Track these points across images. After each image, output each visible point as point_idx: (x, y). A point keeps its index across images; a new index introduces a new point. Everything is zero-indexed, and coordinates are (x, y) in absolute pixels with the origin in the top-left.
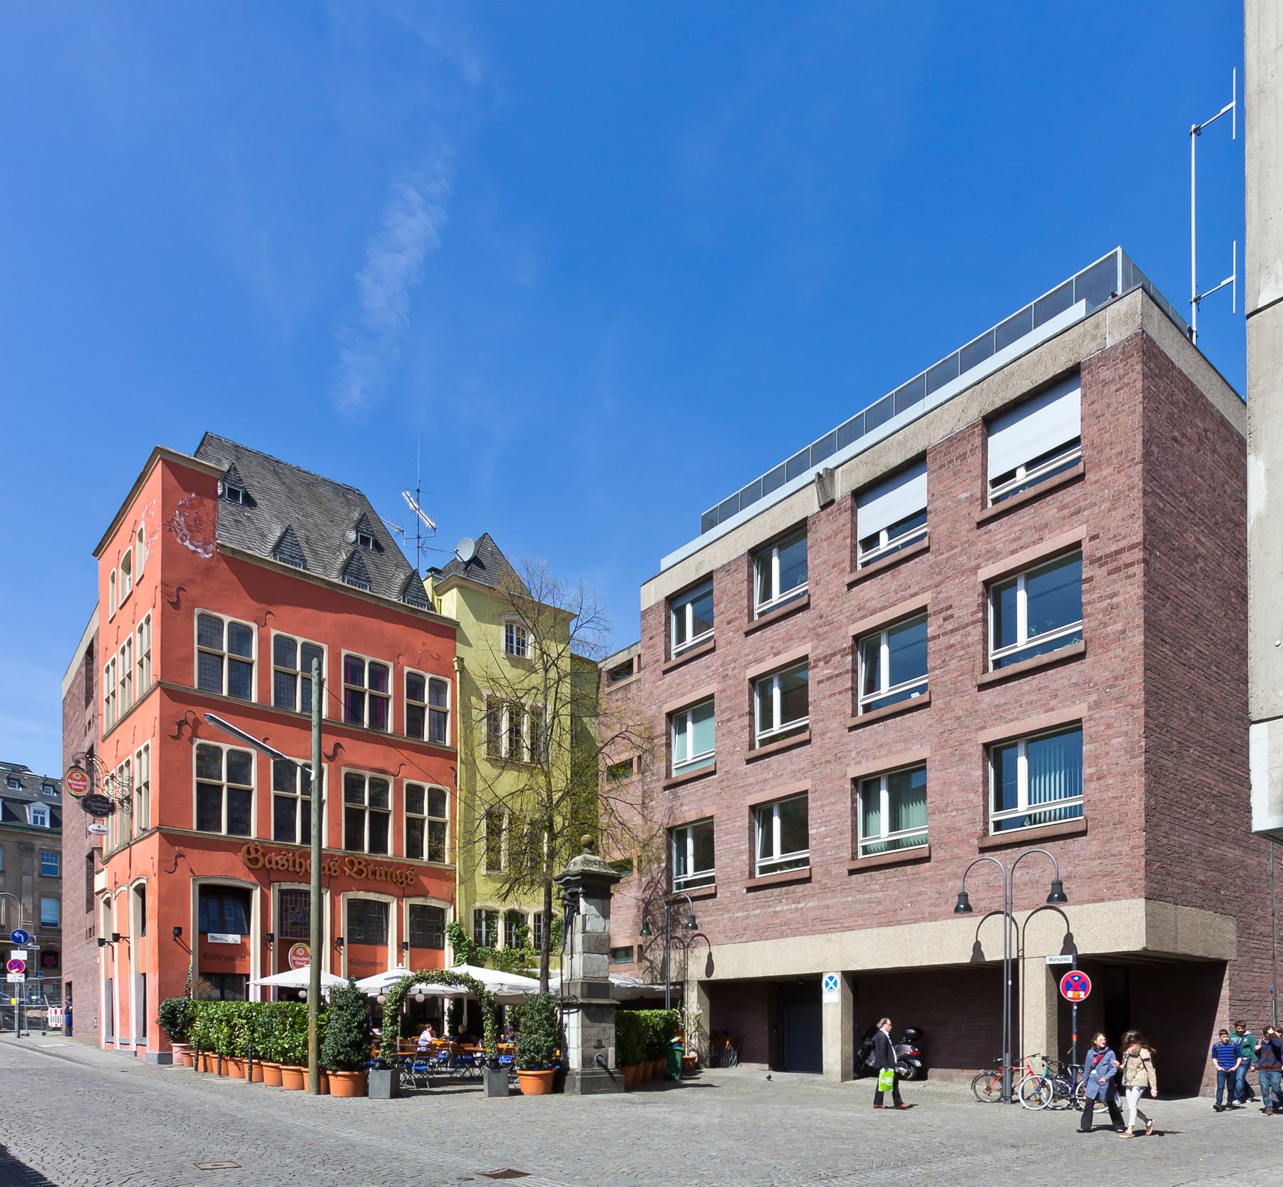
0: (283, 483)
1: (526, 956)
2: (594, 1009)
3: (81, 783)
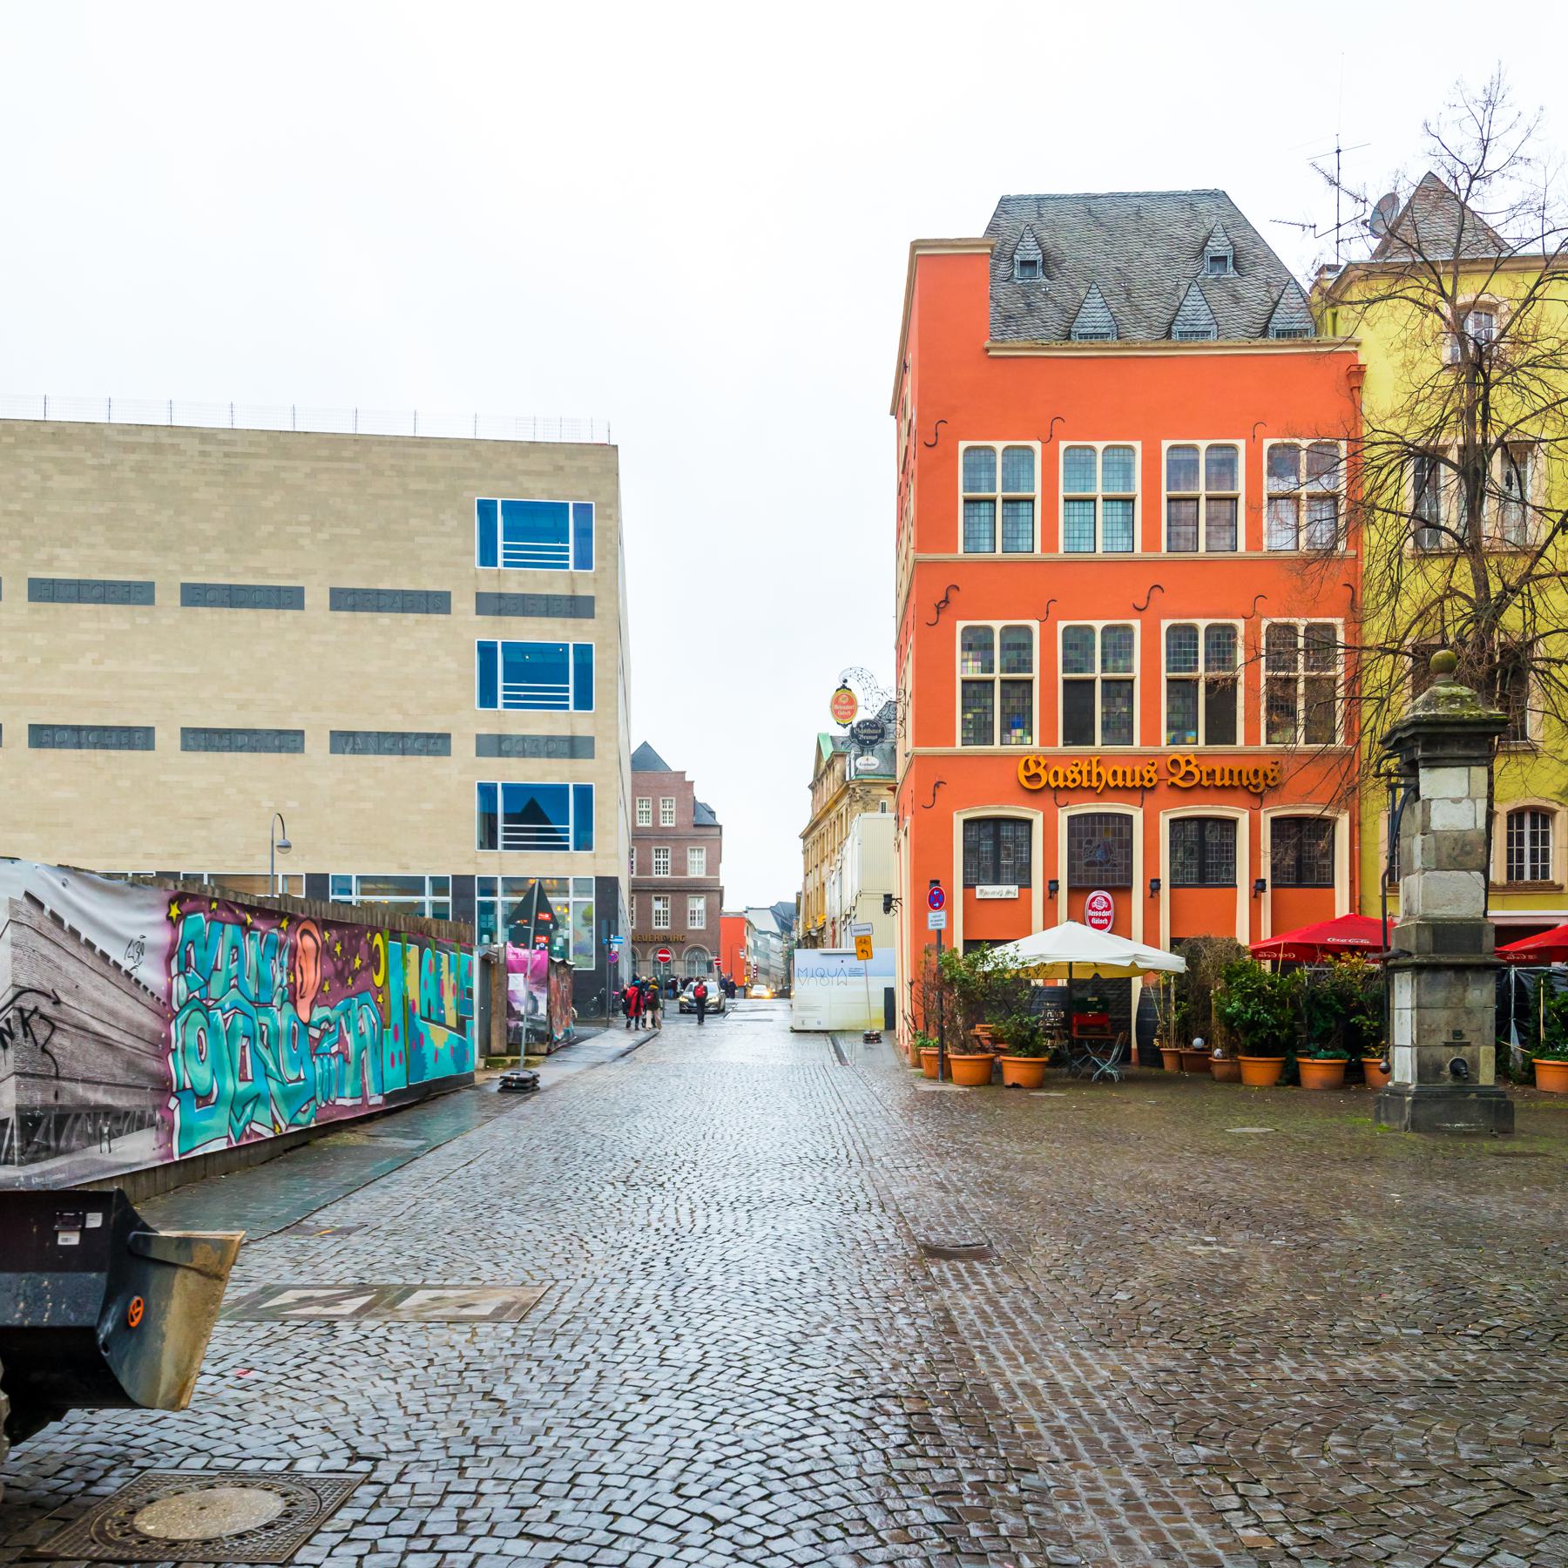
3: (848, 707)
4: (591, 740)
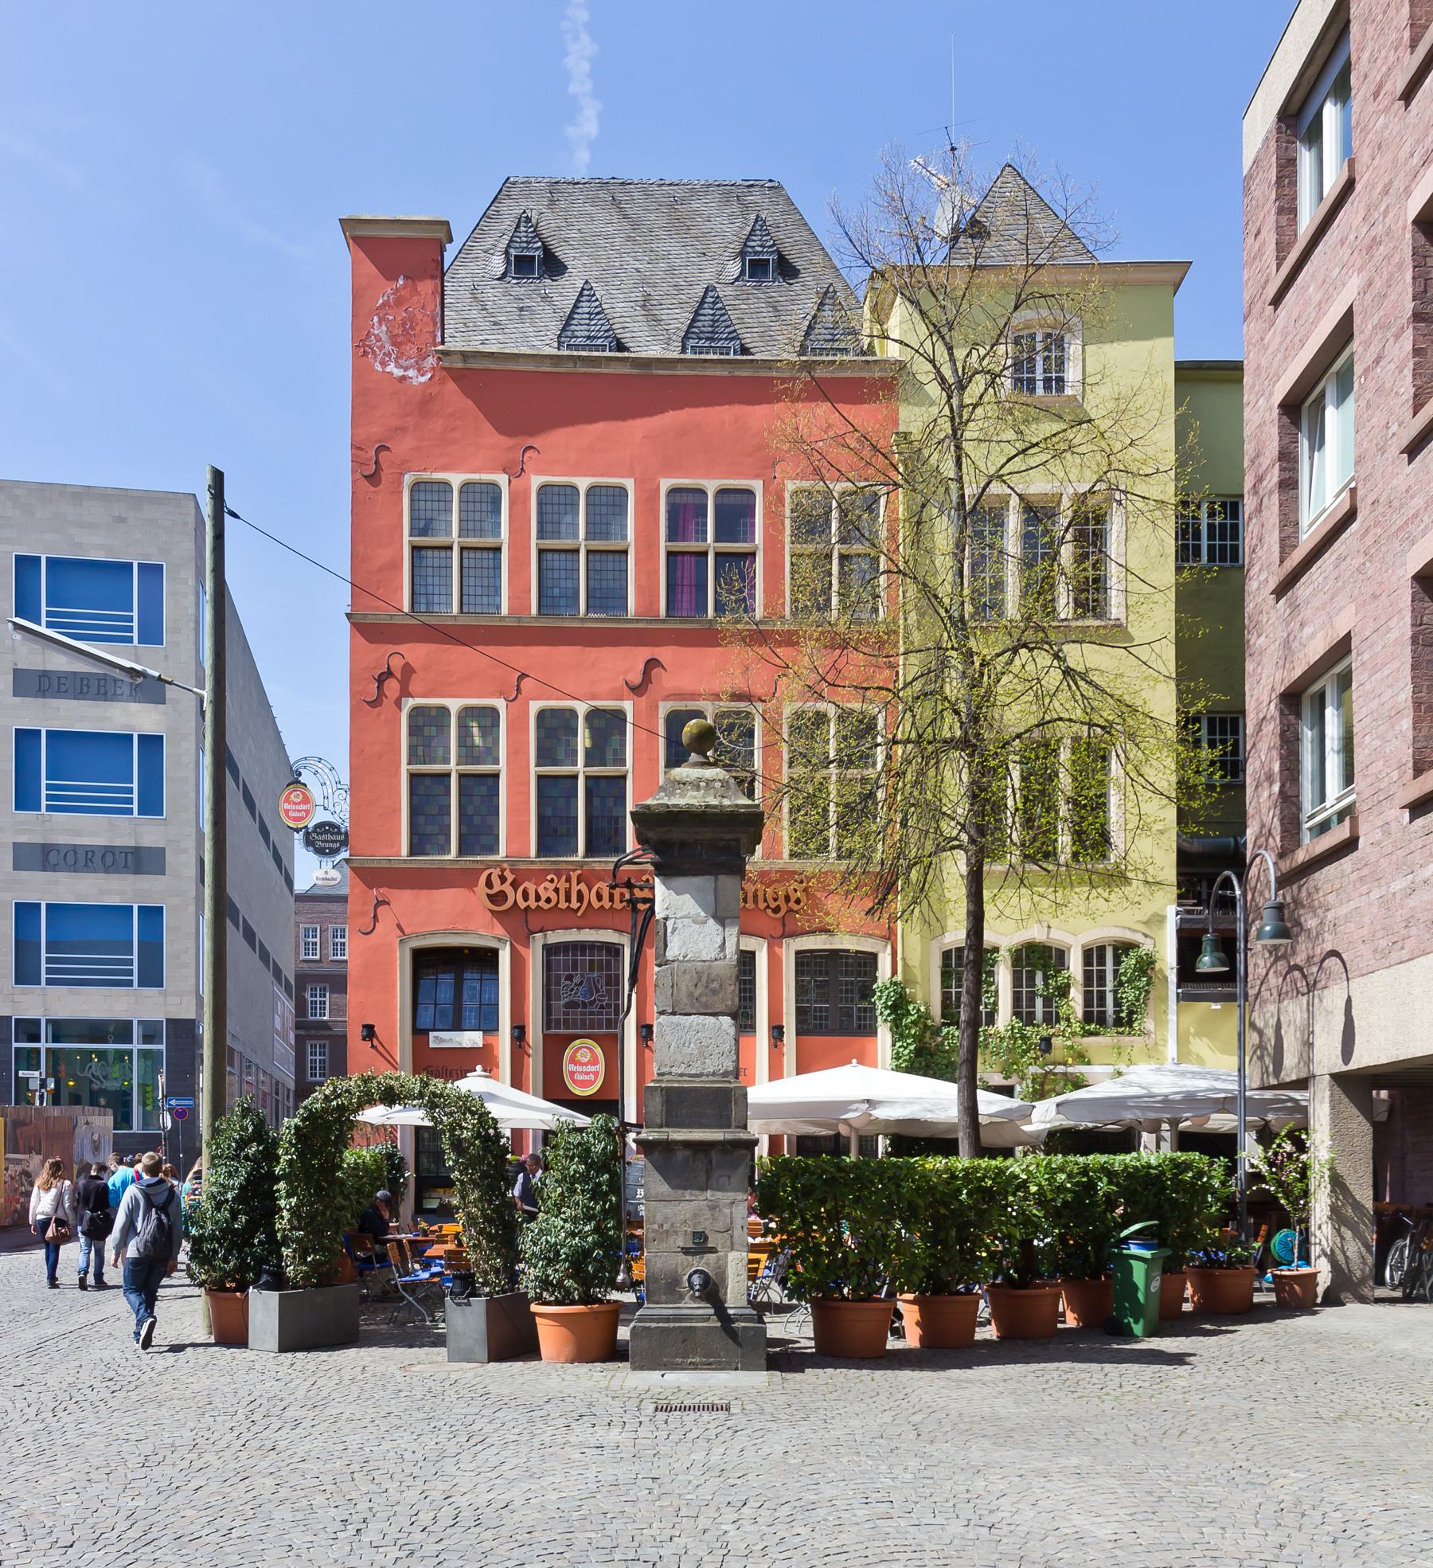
0: (626, 217)
2: (680, 1155)
3: (302, 807)
4: (161, 852)
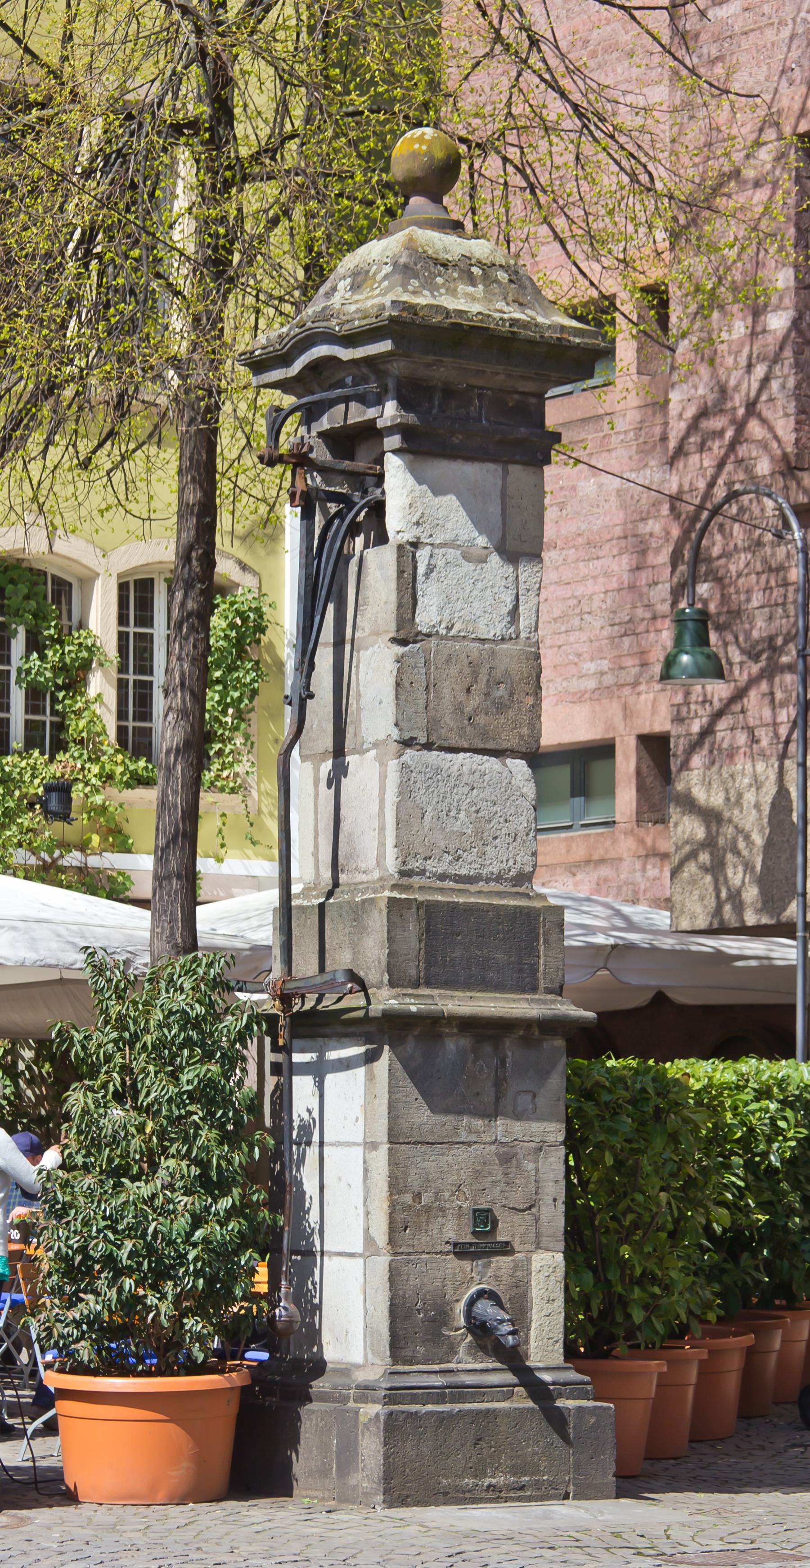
1: (77, 792)
